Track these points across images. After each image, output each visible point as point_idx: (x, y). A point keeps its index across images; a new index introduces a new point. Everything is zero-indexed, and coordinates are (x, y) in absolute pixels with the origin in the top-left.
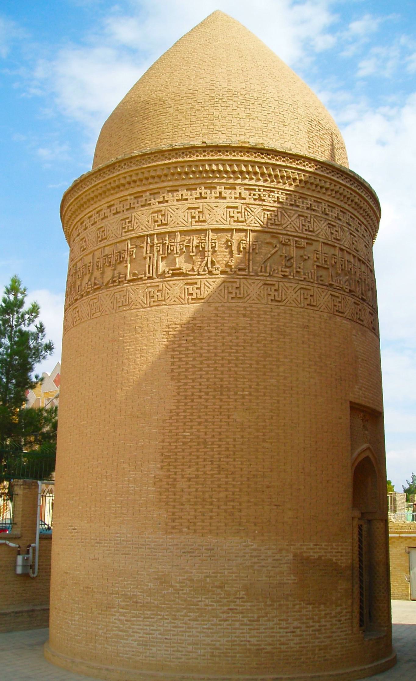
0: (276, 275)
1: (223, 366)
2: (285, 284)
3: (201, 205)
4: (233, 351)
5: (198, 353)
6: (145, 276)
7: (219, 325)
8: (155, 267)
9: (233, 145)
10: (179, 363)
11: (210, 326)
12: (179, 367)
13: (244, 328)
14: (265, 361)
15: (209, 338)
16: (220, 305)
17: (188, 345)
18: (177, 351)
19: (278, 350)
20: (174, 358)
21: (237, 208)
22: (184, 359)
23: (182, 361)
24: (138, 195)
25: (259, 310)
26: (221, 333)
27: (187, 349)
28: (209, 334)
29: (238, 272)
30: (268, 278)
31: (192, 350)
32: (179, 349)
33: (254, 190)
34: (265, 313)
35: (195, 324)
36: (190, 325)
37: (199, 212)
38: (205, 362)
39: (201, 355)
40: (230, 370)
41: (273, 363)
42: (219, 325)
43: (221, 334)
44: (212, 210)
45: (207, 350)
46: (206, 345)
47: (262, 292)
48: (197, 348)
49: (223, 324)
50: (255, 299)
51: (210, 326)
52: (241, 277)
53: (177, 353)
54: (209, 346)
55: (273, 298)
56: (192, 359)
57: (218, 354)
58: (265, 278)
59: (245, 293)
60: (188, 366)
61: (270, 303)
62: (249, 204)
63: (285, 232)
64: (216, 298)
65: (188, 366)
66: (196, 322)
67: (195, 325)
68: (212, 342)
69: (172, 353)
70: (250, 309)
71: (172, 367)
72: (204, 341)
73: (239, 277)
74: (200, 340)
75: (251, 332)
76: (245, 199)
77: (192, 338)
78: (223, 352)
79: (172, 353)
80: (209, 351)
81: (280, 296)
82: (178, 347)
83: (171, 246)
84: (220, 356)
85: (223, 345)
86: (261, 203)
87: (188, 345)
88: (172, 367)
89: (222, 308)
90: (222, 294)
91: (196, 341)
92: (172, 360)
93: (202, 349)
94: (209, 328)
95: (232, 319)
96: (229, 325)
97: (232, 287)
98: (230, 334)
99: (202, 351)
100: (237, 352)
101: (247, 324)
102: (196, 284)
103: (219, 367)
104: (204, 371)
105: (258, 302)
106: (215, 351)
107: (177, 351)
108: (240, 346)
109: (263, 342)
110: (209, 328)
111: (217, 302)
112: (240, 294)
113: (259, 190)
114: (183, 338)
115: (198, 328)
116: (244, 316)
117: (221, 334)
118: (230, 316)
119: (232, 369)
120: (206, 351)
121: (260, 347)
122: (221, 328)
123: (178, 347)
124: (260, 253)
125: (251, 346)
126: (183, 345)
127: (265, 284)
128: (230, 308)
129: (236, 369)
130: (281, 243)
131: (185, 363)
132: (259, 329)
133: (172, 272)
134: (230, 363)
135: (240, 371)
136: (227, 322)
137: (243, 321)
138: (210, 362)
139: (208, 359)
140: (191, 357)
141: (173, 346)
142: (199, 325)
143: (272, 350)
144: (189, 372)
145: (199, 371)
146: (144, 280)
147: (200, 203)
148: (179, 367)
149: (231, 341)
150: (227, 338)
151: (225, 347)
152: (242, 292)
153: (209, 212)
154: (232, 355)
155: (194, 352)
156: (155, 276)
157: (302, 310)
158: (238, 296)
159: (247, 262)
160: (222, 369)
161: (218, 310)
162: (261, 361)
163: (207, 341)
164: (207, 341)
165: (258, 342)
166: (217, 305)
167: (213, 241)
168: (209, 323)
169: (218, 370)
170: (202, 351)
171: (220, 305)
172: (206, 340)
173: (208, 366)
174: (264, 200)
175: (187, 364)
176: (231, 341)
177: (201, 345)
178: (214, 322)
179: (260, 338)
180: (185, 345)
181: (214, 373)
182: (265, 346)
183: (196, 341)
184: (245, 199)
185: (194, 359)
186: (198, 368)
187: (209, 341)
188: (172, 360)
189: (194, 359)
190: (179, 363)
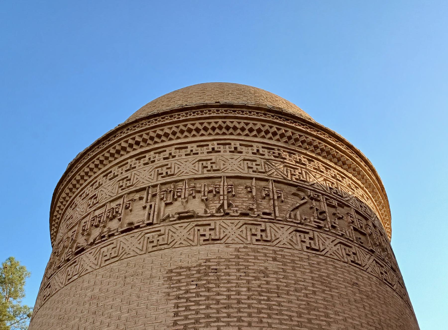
0: (308, 224)
1: (250, 315)
2: (321, 234)
3: (213, 158)
4: (262, 298)
5: (213, 299)
6: (144, 224)
7: (242, 267)
8: (156, 213)
9: (250, 105)
10: (186, 313)
11: (229, 268)
12: (186, 318)
13: (275, 273)
14: (309, 314)
15: (229, 282)
16: (242, 246)
17: (199, 290)
18: (183, 298)
19: (325, 303)
20: (178, 307)
21: (255, 161)
22: (192, 308)
23: (190, 310)
24: (140, 156)
25: (293, 255)
26: (246, 276)
27: (198, 295)
28: (228, 277)
29: (262, 216)
30: (300, 226)
31: (205, 296)
32: (186, 296)
33: (273, 149)
34: (301, 259)
35: (209, 267)
36: (201, 268)
37: (211, 163)
38: (224, 310)
39: (218, 302)
40: (261, 322)
41: (322, 318)
42: (242, 267)
43: (246, 278)
44: (227, 161)
45: (226, 295)
46: (225, 290)
47: (294, 238)
48: (211, 294)
49: (247, 267)
50: (286, 243)
51: (229, 268)
52: (266, 220)
53: (183, 300)
54: (229, 290)
55: (309, 246)
56: (204, 307)
57: (243, 301)
58: (296, 225)
59: (273, 235)
60: (199, 316)
61: (305, 249)
62: (269, 159)
63: (313, 188)
64: (236, 239)
65: (199, 316)
66: (210, 264)
67: (209, 268)
68: (232, 287)
69: (176, 301)
70: (280, 253)
71: (176, 318)
72: (222, 285)
73: (263, 220)
74: (215, 284)
75: (285, 277)
76: (263, 155)
77: (204, 282)
78: (249, 298)
79: (176, 301)
80: (229, 297)
81: (317, 245)
82: (185, 293)
83: (178, 192)
84: (245, 304)
85: (249, 290)
86: (282, 160)
87: (199, 290)
88: (176, 318)
89: (244, 250)
90: (244, 236)
91: (211, 286)
92: (176, 310)
93: (218, 294)
94: (228, 270)
95: (258, 261)
96: (256, 267)
97: (256, 230)
98: (257, 278)
99: (218, 297)
100: (268, 300)
101: (279, 268)
102: (209, 225)
103: (245, 317)
104: (223, 322)
105: (290, 247)
106: (238, 297)
107: (183, 298)
108: (271, 293)
109: (303, 291)
110: (228, 270)
111: (238, 243)
112: (267, 237)
113: (278, 150)
114: (192, 283)
115: (213, 271)
116: (275, 259)
117: (246, 278)
118: (256, 258)
119: (264, 320)
120: (225, 297)
121: (299, 296)
122: (245, 270)
123: (185, 293)
124: (287, 203)
125: (288, 294)
126: (192, 291)
127: (297, 231)
128: (254, 250)
129: (270, 321)
130: (309, 196)
131: (194, 312)
132: (295, 276)
133: (178, 216)
134: (260, 312)
135: (276, 324)
136: (252, 264)
137: (272, 266)
138: (231, 310)
139: (228, 307)
140: (203, 305)
141: (178, 293)
142: (215, 267)
143: (317, 303)
144: (201, 323)
145: (215, 322)
146: (142, 228)
147: (213, 156)
148: (186, 318)
149: (259, 286)
150: (254, 282)
151: (251, 293)
152: (269, 235)
153: (223, 162)
154: (263, 302)
155: (208, 298)
156: (155, 222)
157: (346, 265)
158: (265, 238)
159: (272, 207)
160: (249, 319)
161: (239, 251)
162: (304, 313)
163: (226, 285)
164: (226, 285)
165: (296, 290)
166: (238, 246)
167: (229, 187)
168: (228, 265)
169: (243, 321)
170: (218, 297)
171: (242, 246)
172: (224, 283)
173: (229, 316)
174: (285, 159)
175: (197, 313)
176: (259, 286)
177: (217, 289)
178: (234, 263)
179: (299, 286)
180: (195, 291)
181: (238, 324)
182: (306, 295)
183: (211, 286)
184: (263, 155)
185: (208, 307)
186: (213, 317)
187: (229, 285)
188: (176, 310)
189: (208, 307)
190: (186, 313)
